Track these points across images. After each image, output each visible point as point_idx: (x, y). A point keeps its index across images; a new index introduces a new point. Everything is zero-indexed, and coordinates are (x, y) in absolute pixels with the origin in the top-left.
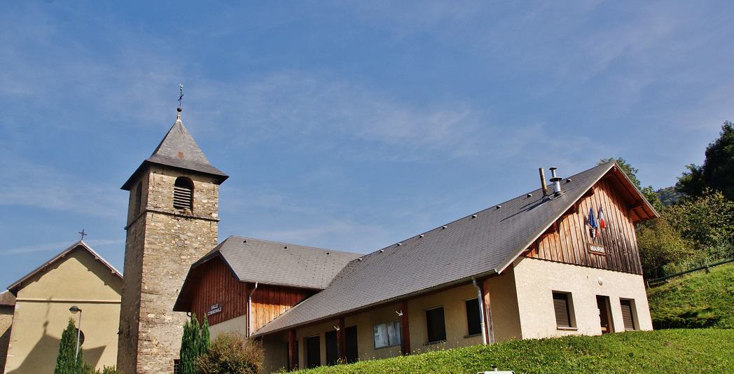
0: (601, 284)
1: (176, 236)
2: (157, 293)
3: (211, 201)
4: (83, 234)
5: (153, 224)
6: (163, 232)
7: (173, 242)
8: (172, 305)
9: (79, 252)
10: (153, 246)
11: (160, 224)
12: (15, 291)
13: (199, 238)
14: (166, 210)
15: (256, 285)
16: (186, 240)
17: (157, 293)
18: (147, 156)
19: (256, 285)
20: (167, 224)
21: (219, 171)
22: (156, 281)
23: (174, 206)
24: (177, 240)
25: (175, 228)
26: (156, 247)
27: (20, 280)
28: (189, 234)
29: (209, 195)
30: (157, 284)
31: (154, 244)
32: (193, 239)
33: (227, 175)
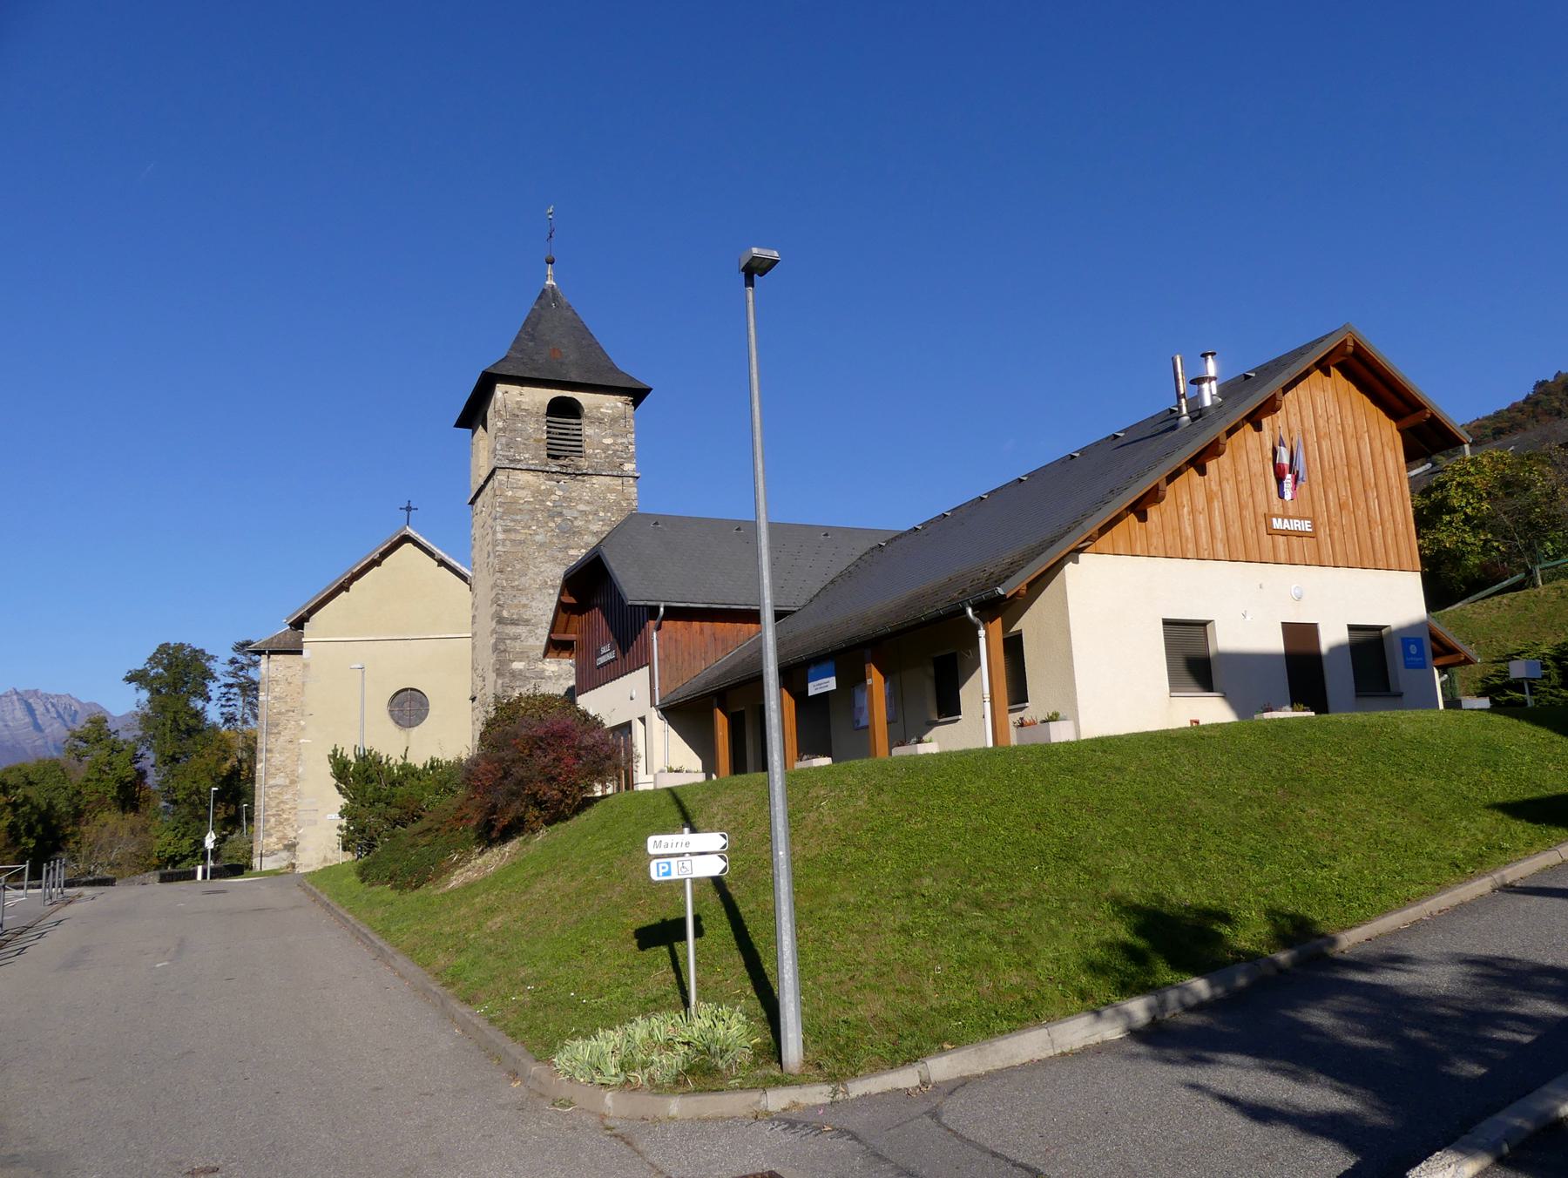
0: (632, 699)
1: (553, 514)
2: (527, 622)
3: (620, 441)
4: (409, 509)
5: (510, 493)
6: (530, 507)
7: (552, 524)
8: (1225, 438)
9: (406, 539)
10: (513, 536)
11: (521, 493)
12: (298, 624)
13: (601, 514)
14: (534, 463)
15: (662, 609)
16: (576, 518)
17: (527, 622)
18: (486, 364)
19: (662, 609)
20: (537, 492)
21: (632, 379)
22: (524, 601)
23: (549, 456)
24: (558, 520)
25: (553, 497)
26: (519, 537)
27: (305, 606)
28: (582, 507)
29: (617, 429)
30: (524, 606)
31: (516, 531)
32: (591, 517)
33: (651, 386)
